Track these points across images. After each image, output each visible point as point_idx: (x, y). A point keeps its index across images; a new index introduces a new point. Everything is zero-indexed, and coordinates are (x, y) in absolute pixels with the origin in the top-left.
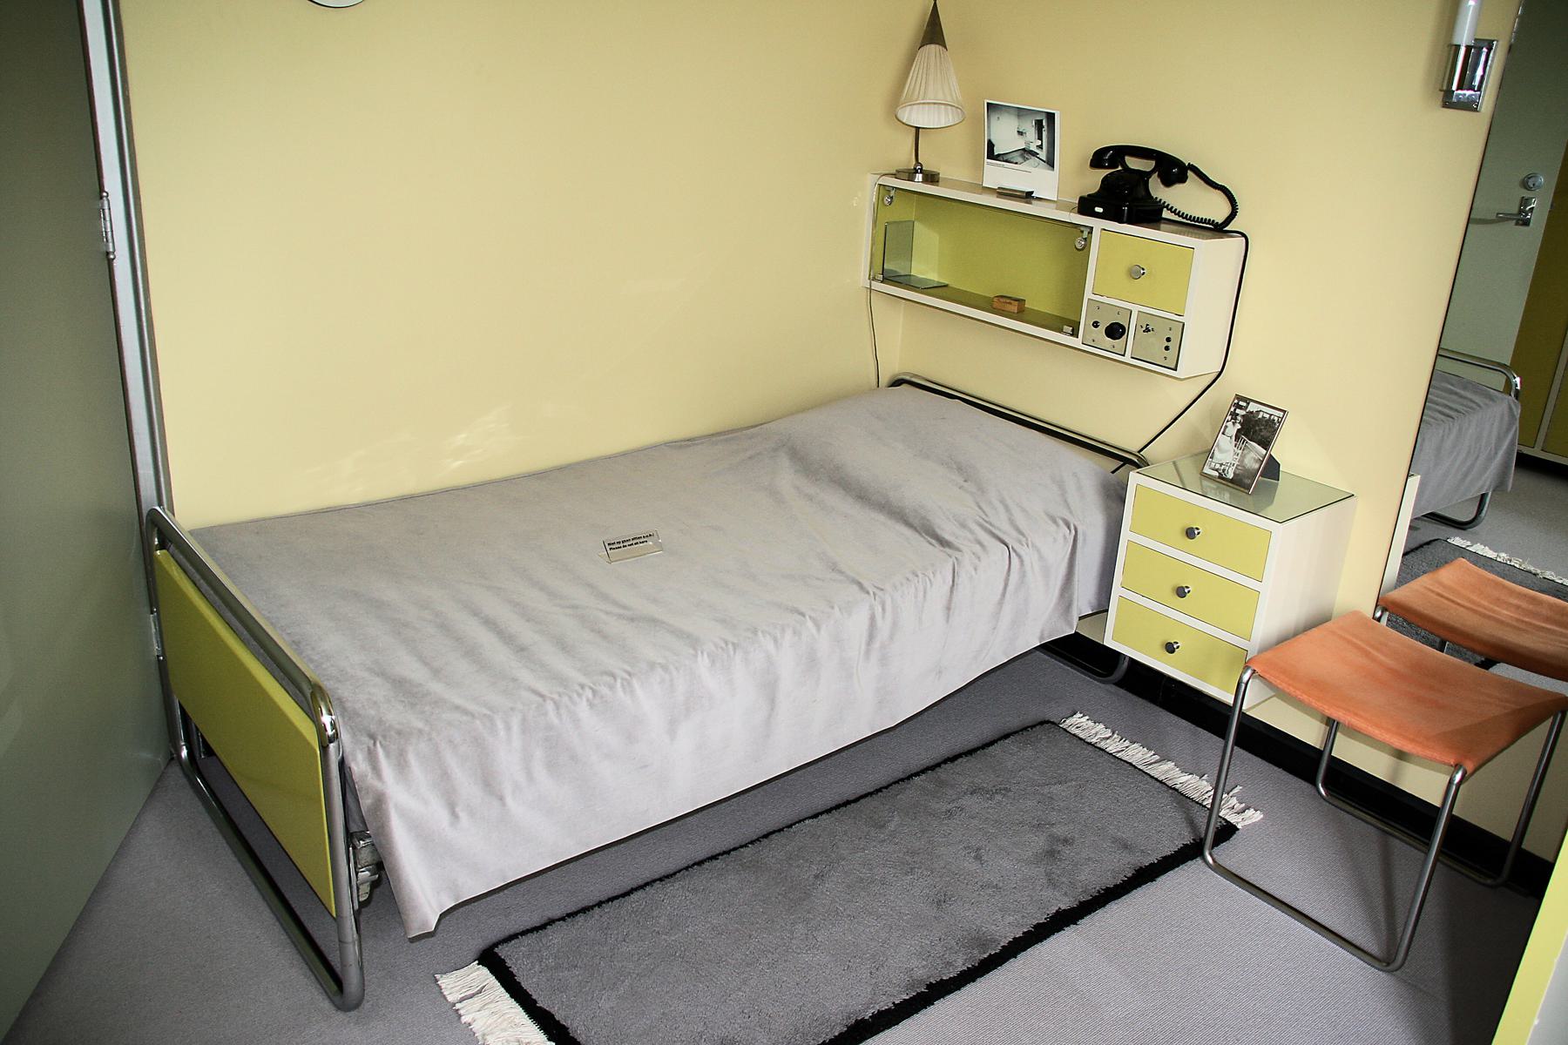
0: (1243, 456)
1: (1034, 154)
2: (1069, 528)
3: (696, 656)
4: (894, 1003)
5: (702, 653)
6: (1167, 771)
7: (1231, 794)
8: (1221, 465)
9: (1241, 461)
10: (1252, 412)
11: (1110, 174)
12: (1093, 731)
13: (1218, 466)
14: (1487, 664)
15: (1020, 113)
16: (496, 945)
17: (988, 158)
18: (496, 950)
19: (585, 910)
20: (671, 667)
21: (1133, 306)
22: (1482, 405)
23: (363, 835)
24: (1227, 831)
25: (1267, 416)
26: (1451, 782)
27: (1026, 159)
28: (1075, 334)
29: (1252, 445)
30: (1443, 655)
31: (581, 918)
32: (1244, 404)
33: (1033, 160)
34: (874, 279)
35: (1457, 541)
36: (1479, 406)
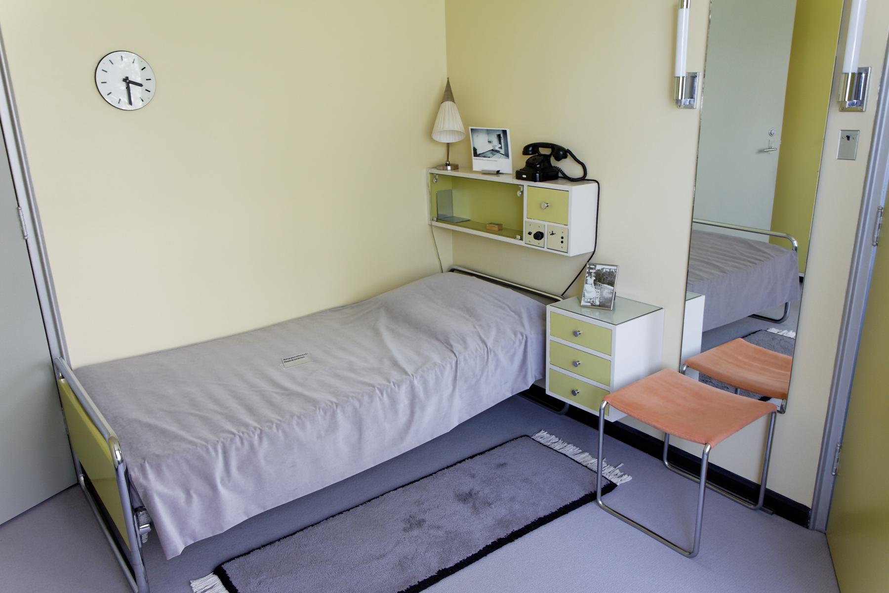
0: (602, 293)
1: (497, 152)
2: (523, 336)
4: (418, 582)
5: (319, 409)
6: (584, 458)
7: (617, 468)
8: (591, 299)
9: (601, 295)
10: (599, 270)
11: (531, 158)
12: (549, 439)
13: (589, 300)
15: (489, 132)
17: (474, 156)
18: (223, 566)
19: (271, 543)
20: (302, 417)
22: (774, 256)
23: (142, 508)
24: (610, 487)
25: (608, 270)
27: (494, 155)
28: (521, 239)
29: (604, 286)
30: (737, 396)
31: (268, 547)
32: (593, 267)
33: (498, 155)
34: (433, 220)
35: (774, 330)
36: (772, 257)
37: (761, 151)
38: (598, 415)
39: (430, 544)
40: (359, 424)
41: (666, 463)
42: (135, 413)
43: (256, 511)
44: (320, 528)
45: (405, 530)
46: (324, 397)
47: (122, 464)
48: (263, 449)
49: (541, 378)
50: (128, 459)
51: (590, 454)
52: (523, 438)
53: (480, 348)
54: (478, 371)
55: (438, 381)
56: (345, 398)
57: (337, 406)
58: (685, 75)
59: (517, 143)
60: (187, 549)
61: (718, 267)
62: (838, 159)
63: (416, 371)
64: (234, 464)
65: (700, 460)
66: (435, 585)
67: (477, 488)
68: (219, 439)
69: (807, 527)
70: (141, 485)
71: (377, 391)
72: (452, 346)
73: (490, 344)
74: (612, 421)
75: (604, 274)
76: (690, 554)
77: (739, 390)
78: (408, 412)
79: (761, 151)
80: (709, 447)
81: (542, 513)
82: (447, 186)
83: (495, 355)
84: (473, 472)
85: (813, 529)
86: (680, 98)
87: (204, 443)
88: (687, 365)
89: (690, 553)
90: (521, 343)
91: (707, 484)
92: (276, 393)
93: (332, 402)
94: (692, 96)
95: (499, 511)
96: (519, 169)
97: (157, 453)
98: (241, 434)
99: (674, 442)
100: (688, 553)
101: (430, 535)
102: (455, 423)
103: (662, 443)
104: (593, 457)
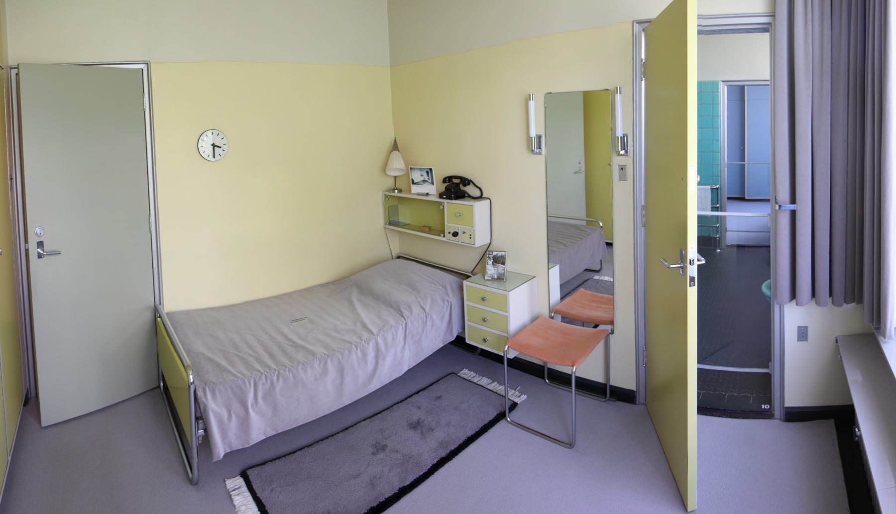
0: (498, 270)
3: (314, 360)
4: (385, 498)
13: (490, 276)
14: (596, 326)
15: (421, 169)
16: (247, 469)
20: (305, 364)
21: (459, 228)
24: (514, 406)
26: (47, 255)
27: (424, 183)
28: (444, 236)
30: (585, 328)
31: (277, 461)
33: (427, 183)
35: (596, 277)
37: (576, 173)
38: (503, 355)
39: (391, 465)
40: (341, 372)
41: (547, 381)
42: (202, 350)
43: (271, 433)
44: (313, 449)
45: (373, 454)
46: (319, 350)
47: (193, 385)
48: (280, 385)
49: (462, 330)
50: (196, 382)
51: (498, 383)
52: (452, 375)
53: (421, 313)
54: (420, 330)
55: (394, 338)
56: (332, 352)
57: (328, 357)
59: (438, 176)
60: (226, 455)
61: (562, 243)
63: (379, 332)
64: (260, 395)
65: (571, 376)
66: (397, 503)
67: (423, 418)
68: (252, 375)
69: (636, 404)
70: (203, 402)
71: (354, 347)
72: (402, 312)
73: (427, 310)
74: (511, 358)
75: (498, 257)
76: (570, 445)
77: (585, 324)
78: (374, 362)
79: (576, 173)
80: (575, 367)
81: (470, 433)
82: (396, 202)
83: (431, 317)
84: (419, 405)
85: (639, 404)
86: (533, 149)
87: (242, 377)
88: (554, 311)
89: (570, 445)
90: (447, 307)
91: (576, 392)
92: (287, 345)
93: (323, 353)
94: (540, 148)
95: (439, 435)
96: (440, 192)
97: (214, 381)
98: (266, 373)
99: (550, 366)
100: (569, 446)
101: (391, 458)
102: (406, 368)
103: (543, 367)
104: (501, 384)
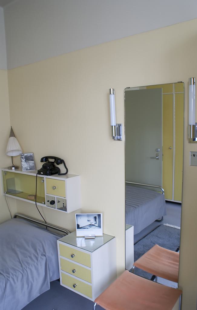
17: (77, 229)
28: (45, 204)
33: (93, 227)
58: (115, 125)
59: (38, 158)
62: (191, 165)
86: (114, 136)
94: (119, 135)
